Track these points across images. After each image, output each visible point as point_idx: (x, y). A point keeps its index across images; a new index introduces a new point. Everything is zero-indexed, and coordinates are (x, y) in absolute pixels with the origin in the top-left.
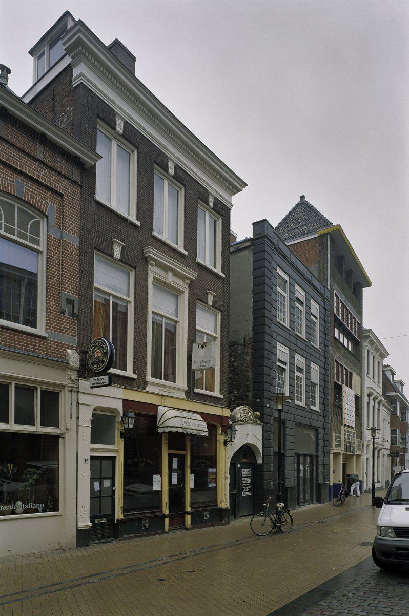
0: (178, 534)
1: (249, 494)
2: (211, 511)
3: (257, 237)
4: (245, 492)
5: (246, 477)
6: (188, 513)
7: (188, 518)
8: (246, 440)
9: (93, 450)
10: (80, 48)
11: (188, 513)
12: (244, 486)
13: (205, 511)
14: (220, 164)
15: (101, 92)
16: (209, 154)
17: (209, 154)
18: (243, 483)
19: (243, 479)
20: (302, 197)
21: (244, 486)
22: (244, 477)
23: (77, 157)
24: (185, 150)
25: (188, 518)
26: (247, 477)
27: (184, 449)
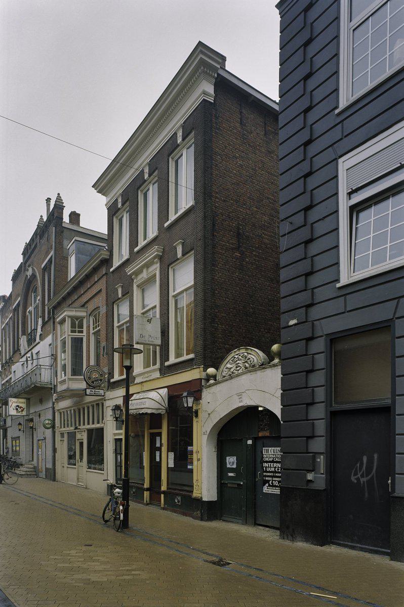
0: (152, 509)
1: (277, 491)
2: (183, 497)
3: (283, 13)
4: (269, 485)
5: (273, 462)
6: (147, 490)
7: (146, 494)
8: (240, 402)
9: (115, 434)
10: (202, 68)
11: (164, 492)
12: (268, 476)
13: (178, 495)
14: (157, 108)
15: (160, 142)
16: (169, 91)
17: (169, 91)
18: (266, 472)
19: (265, 465)
20: (59, 194)
21: (268, 476)
22: (267, 462)
23: (74, 287)
24: (162, 124)
25: (146, 494)
26: (277, 462)
27: (161, 428)
